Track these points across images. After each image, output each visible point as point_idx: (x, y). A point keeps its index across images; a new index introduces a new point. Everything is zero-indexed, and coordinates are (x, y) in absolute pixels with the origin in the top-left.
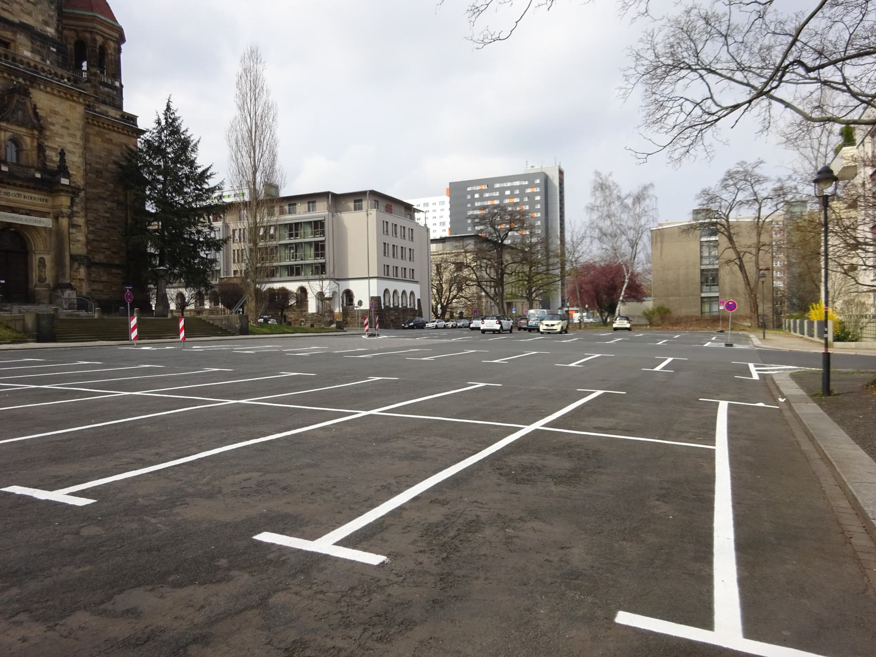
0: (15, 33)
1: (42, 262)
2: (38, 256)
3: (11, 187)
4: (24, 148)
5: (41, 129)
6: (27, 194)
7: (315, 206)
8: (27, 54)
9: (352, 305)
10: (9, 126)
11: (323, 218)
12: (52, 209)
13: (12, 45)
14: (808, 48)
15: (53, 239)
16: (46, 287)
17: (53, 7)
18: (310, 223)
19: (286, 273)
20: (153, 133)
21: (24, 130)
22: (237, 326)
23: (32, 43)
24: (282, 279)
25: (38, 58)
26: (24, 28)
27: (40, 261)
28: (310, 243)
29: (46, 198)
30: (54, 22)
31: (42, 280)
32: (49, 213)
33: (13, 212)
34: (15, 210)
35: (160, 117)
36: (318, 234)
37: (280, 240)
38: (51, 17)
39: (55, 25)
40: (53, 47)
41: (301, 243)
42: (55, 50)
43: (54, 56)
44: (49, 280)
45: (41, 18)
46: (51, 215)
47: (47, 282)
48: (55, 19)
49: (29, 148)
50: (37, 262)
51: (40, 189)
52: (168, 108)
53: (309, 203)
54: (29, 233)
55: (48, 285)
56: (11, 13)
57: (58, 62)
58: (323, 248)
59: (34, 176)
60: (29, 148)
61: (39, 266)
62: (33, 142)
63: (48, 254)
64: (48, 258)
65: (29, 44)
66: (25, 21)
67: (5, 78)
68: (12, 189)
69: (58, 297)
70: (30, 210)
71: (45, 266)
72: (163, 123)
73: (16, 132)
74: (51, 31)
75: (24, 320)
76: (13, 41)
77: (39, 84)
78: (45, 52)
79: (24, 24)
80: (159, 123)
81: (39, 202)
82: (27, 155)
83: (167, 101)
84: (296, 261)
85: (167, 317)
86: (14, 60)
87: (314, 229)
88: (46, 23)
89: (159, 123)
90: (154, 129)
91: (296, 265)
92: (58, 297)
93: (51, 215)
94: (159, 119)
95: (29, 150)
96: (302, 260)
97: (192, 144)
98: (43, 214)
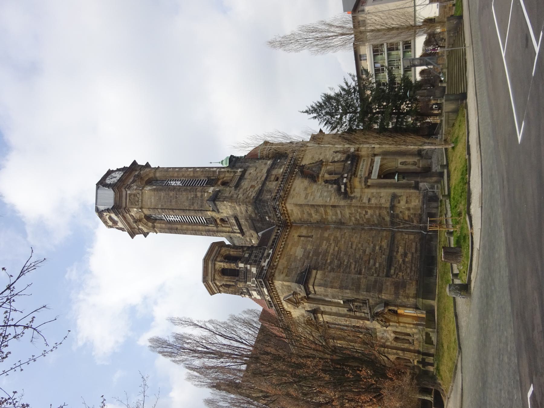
0: (272, 175)
1: (402, 163)
2: (399, 165)
3: (356, 173)
4: (333, 169)
5: (321, 162)
6: (361, 167)
7: (363, 55)
8: (282, 170)
9: (434, 19)
10: (322, 174)
11: (371, 46)
12: (369, 157)
13: (278, 176)
14: (157, 212)
15: (388, 157)
16: (420, 161)
17: (257, 161)
18: (374, 56)
19: (409, 72)
20: (321, 121)
21: (323, 169)
22: (455, 22)
23: (276, 168)
24: (413, 74)
25: (283, 166)
26: (269, 171)
27: (403, 164)
28: (389, 55)
29: (362, 160)
30: (265, 161)
31: (415, 164)
32: (372, 159)
33: (371, 173)
34: (370, 171)
35: (312, 117)
36: (382, 49)
37: (386, 78)
38: (262, 162)
39: (266, 161)
40: (277, 161)
41: (388, 61)
42: (279, 160)
43: (282, 160)
44: (416, 159)
45: (263, 166)
46: (373, 158)
47: (416, 161)
48: (263, 161)
49: (333, 167)
50: (403, 166)
51: (358, 161)
52: (307, 112)
53: (361, 60)
54: (384, 170)
55: (418, 160)
56: (262, 176)
57: (285, 159)
58: (392, 44)
59: (349, 164)
60: (333, 167)
61: (406, 165)
62: (330, 165)
63: (398, 160)
64: (400, 160)
65: (277, 170)
66: (266, 171)
67: (295, 176)
68: (358, 173)
69: (427, 153)
70: (370, 166)
71: (405, 162)
72: (315, 115)
73: (324, 171)
74: (269, 162)
75: (448, 112)
76: (276, 176)
77: (297, 163)
78: (280, 164)
79: (267, 172)
80: (315, 117)
81: (365, 163)
82: (337, 168)
83: (302, 113)
84: (400, 65)
85: (445, 87)
86: (285, 173)
87: (378, 52)
88: (266, 164)
89: (315, 117)
90: (319, 120)
91: (403, 50)
92: (427, 153)
93: (373, 158)
94: (313, 117)
95: (334, 167)
96: (400, 60)
97: (311, 209)
98: (372, 162)
